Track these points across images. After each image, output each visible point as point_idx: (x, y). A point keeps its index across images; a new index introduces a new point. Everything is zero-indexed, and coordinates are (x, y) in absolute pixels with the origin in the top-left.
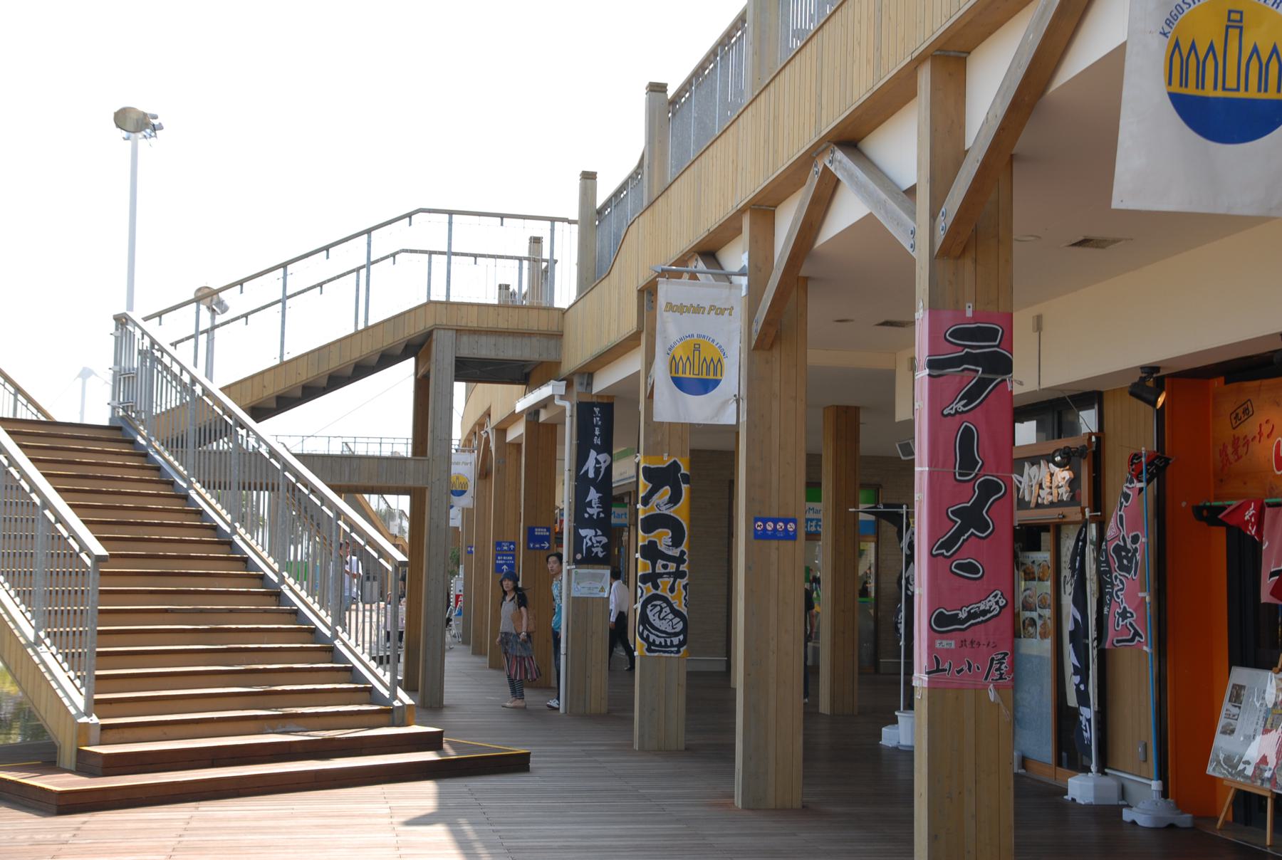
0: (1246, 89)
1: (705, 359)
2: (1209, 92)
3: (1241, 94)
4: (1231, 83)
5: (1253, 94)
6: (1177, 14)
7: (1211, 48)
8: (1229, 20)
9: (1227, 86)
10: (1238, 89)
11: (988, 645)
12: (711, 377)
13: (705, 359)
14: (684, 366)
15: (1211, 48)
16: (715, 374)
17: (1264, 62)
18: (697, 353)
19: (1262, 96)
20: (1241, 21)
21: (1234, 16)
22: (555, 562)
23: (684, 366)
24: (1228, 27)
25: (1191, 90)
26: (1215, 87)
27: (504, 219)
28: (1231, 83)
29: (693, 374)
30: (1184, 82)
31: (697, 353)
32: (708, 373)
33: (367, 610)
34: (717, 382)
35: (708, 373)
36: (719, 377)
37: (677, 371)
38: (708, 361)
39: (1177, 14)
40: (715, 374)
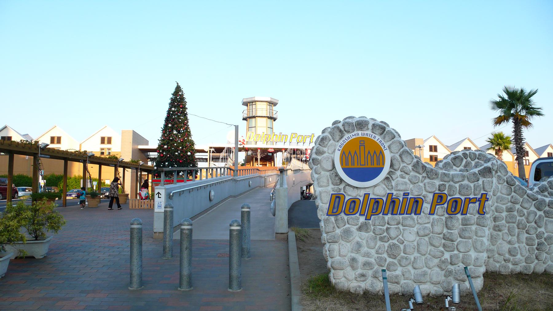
0: (368, 165)
1: (369, 152)
2: (356, 166)
3: (366, 166)
4: (363, 163)
5: (370, 166)
6: (343, 143)
7: (355, 152)
8: (360, 144)
9: (361, 164)
10: (365, 165)
11: (436, 302)
12: (375, 166)
13: (369, 152)
14: (353, 159)
15: (355, 152)
16: (378, 163)
17: (372, 156)
18: (362, 148)
19: (372, 166)
20: (364, 144)
21: (361, 142)
22: (412, 300)
23: (353, 159)
24: (360, 146)
25: (350, 166)
26: (358, 165)
27: (103, 166)
28: (363, 163)
29: (361, 165)
30: (347, 164)
31: (362, 148)
32: (372, 163)
33: (95, 180)
34: (383, 168)
35: (372, 163)
36: (381, 166)
37: (347, 164)
38: (372, 153)
39: (343, 143)
40: (378, 163)
